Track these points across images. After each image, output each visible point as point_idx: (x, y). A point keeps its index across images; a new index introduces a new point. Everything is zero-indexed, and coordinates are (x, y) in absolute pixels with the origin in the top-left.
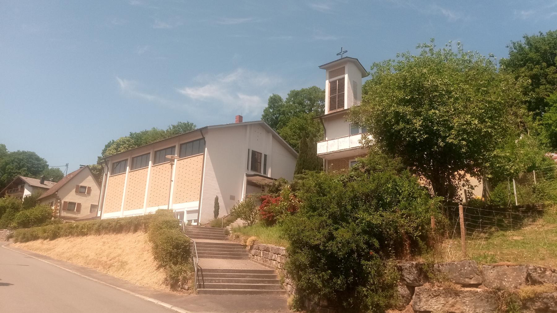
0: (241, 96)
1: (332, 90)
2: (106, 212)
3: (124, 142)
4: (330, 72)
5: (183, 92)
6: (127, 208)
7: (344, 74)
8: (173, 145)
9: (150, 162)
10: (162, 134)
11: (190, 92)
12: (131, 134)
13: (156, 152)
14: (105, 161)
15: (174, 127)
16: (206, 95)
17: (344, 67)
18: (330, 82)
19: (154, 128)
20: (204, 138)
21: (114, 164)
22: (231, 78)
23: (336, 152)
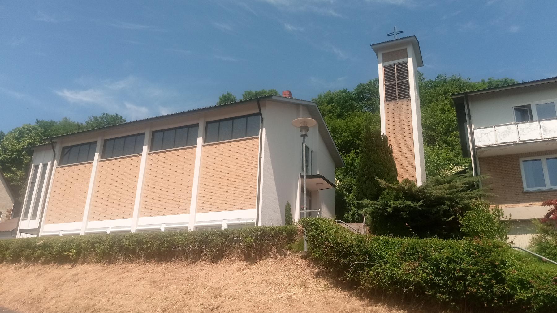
0: (128, 105)
1: (389, 76)
2: (48, 222)
3: (29, 130)
4: (383, 54)
5: (60, 94)
6: (94, 216)
7: (407, 57)
8: (195, 122)
9: (97, 155)
10: (79, 126)
11: (68, 94)
12: (38, 122)
13: (106, 141)
14: (52, 144)
15: (96, 119)
16: (86, 99)
17: (406, 49)
18: (383, 66)
19: (66, 118)
20: (260, 114)
21: (64, 148)
22: (121, 85)
23: (492, 147)
